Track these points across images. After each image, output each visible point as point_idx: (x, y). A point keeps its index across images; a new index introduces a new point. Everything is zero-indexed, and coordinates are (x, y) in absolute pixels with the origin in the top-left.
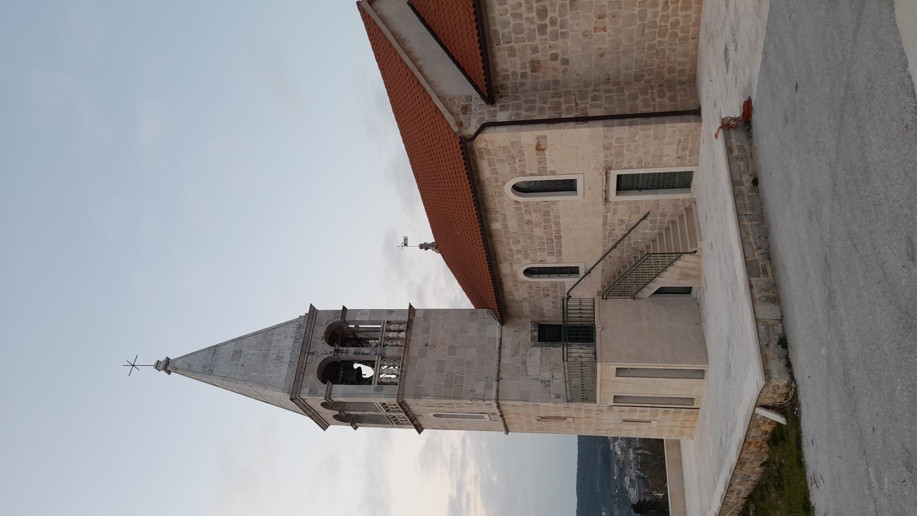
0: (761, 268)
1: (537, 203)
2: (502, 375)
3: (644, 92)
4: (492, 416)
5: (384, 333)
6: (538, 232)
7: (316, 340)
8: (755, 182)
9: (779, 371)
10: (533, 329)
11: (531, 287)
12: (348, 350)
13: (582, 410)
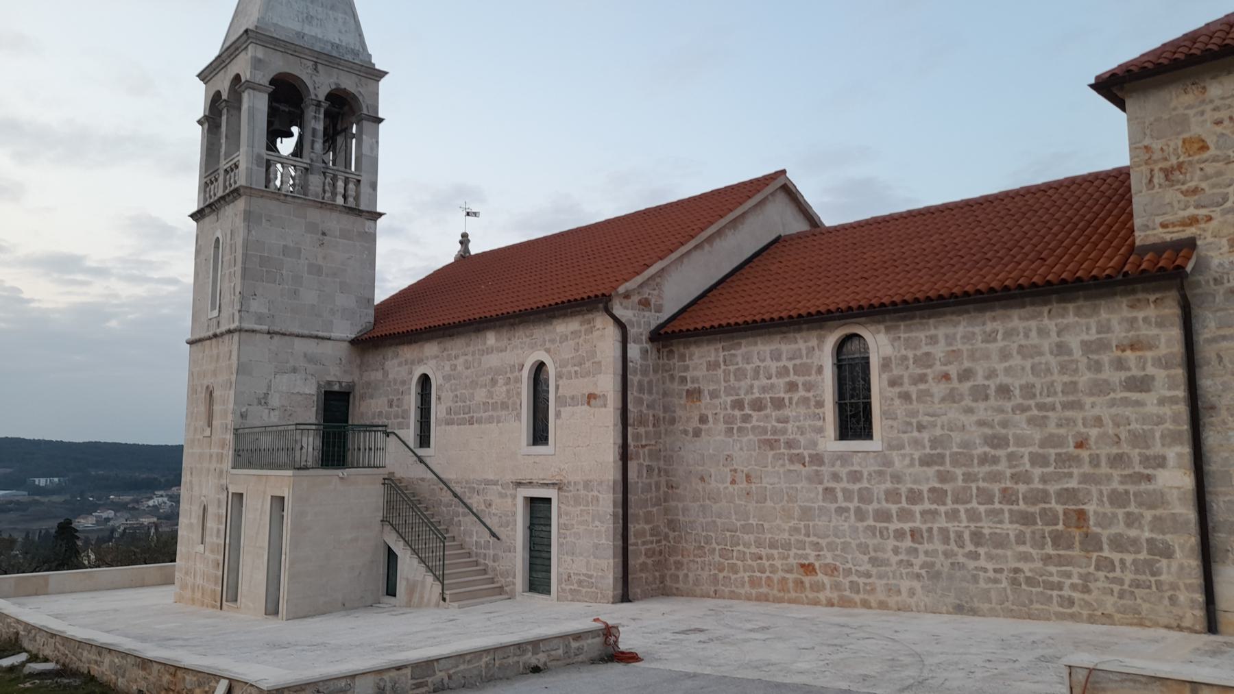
1: (519, 394)
2: (276, 338)
3: (655, 532)
4: (215, 321)
6: (480, 395)
8: (536, 670)
10: (344, 384)
11: (403, 383)
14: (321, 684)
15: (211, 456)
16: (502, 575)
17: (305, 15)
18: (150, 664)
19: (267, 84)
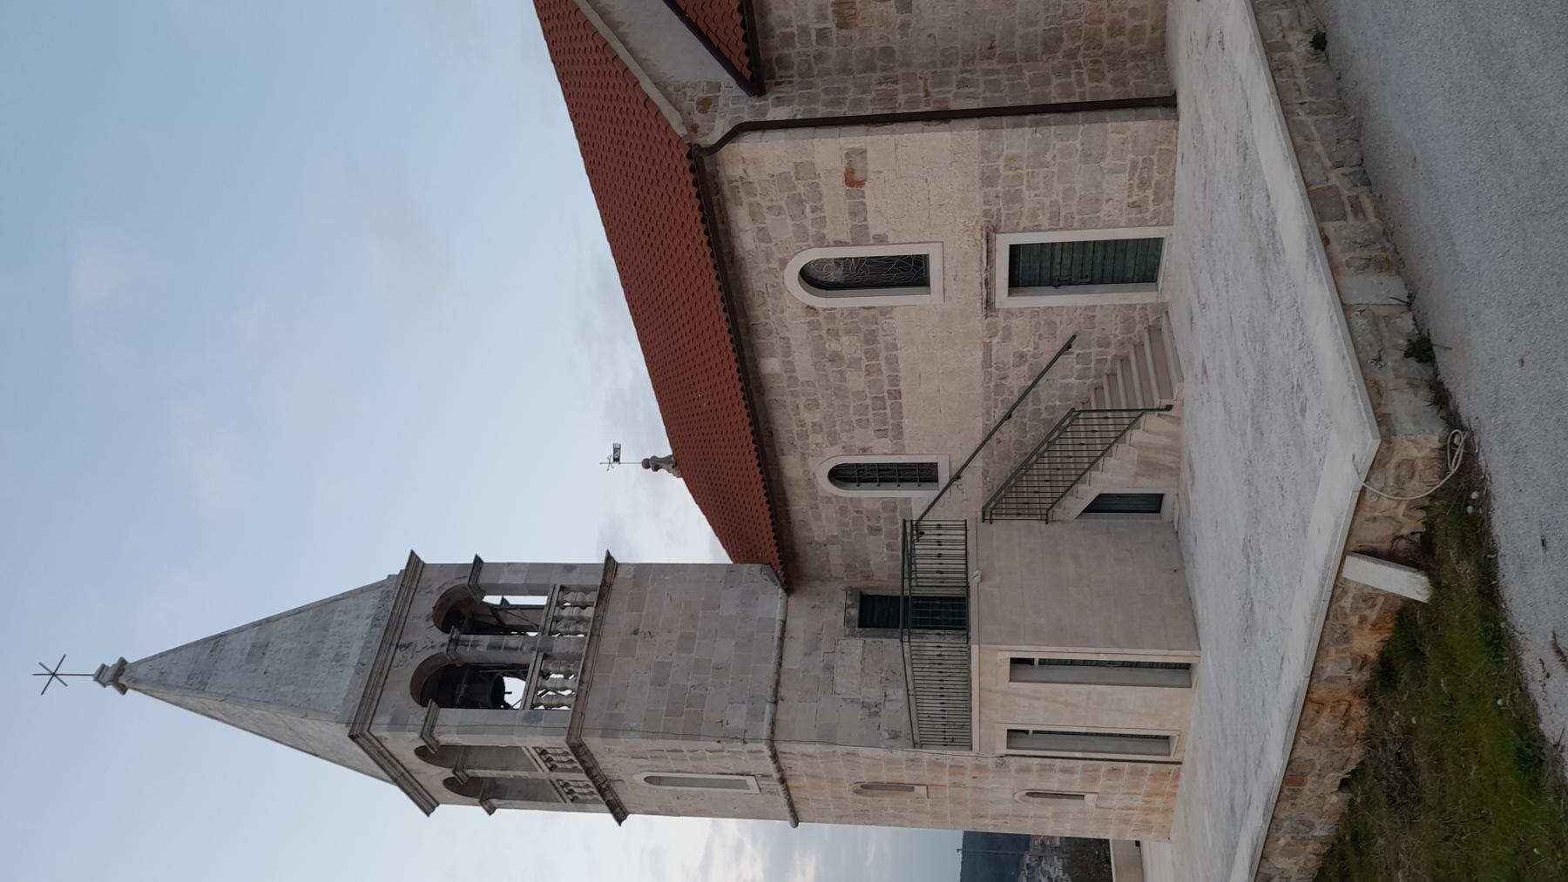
0: (1347, 202)
1: (852, 312)
2: (783, 692)
3: (1063, 72)
4: (763, 782)
5: (552, 608)
6: (856, 380)
7: (415, 621)
8: (1319, 42)
9: (1414, 416)
10: (849, 602)
11: (843, 511)
12: (477, 641)
13: (945, 766)
14: (1362, 355)
15: (955, 785)
16: (1129, 330)
17: (334, 663)
18: (1294, 766)
19: (426, 710)
